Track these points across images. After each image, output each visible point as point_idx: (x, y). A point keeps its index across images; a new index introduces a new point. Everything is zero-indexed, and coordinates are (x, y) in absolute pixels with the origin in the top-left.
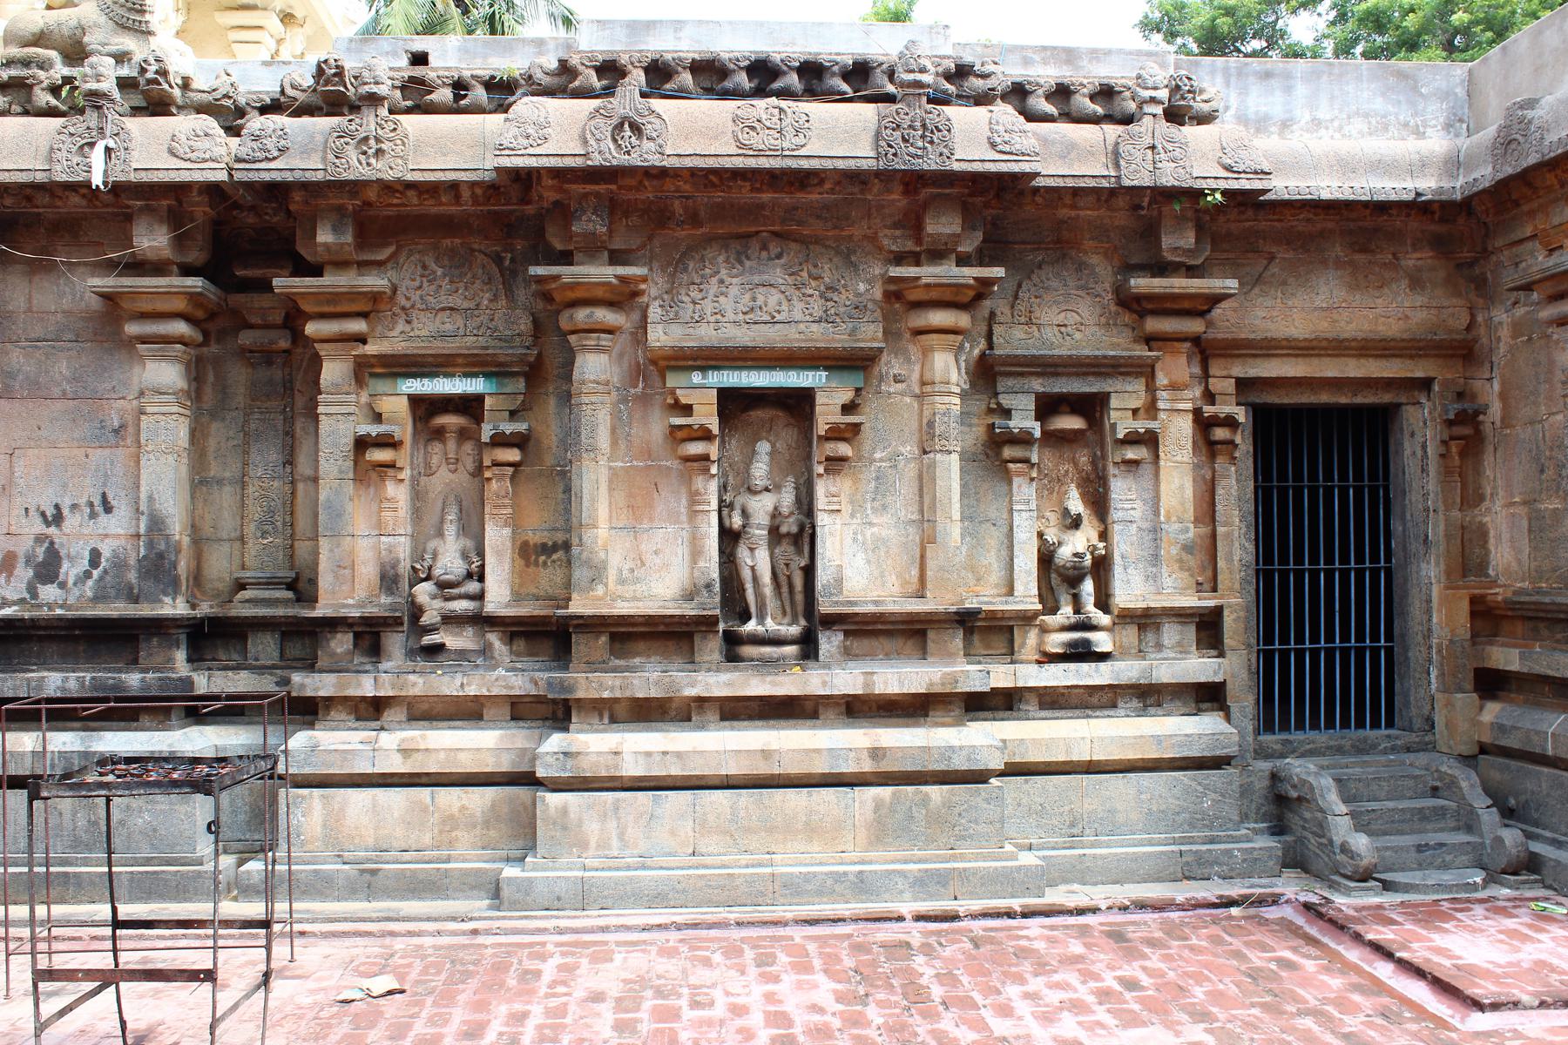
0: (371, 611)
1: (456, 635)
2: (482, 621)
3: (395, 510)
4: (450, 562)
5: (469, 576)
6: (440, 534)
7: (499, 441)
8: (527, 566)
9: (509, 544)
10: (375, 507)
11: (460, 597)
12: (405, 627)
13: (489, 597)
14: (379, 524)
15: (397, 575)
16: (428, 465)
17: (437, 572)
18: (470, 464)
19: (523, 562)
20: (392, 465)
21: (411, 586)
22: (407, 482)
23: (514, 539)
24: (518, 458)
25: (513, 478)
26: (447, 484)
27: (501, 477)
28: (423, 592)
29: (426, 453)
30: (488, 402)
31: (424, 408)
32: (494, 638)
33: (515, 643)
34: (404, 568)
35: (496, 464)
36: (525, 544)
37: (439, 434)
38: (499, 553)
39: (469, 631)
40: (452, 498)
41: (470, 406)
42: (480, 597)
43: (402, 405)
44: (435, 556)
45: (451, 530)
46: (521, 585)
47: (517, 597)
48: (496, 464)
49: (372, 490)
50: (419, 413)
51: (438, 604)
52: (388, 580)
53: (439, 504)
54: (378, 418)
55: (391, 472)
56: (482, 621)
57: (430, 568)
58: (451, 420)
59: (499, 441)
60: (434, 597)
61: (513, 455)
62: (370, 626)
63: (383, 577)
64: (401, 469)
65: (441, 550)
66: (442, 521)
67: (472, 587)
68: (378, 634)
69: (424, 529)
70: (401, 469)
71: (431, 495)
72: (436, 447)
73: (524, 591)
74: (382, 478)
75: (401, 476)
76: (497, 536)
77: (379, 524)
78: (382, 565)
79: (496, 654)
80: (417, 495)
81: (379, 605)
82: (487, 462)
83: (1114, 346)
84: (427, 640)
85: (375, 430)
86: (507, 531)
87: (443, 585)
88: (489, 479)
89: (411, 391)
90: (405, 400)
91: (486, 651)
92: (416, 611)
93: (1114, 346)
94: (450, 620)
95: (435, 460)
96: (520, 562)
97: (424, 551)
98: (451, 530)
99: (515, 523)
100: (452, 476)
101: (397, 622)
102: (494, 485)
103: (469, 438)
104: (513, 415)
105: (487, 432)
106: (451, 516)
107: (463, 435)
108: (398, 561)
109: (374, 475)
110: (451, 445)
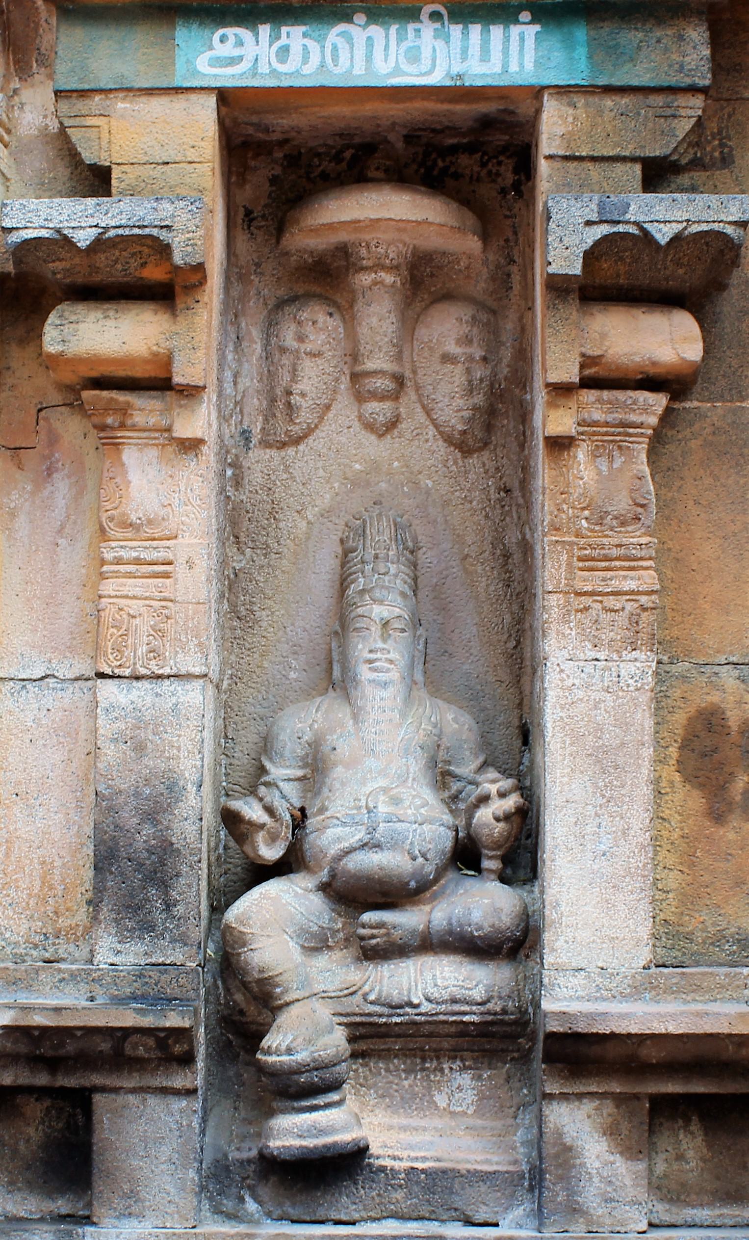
0: (58, 1002)
1: (405, 1102)
2: (518, 1047)
3: (163, 569)
4: (384, 792)
5: (465, 855)
6: (334, 675)
7: (622, 276)
8: (718, 817)
9: (644, 720)
10: (72, 560)
11: (429, 944)
12: (198, 1075)
13: (559, 947)
14: (93, 629)
15: (166, 850)
16: (279, 401)
17: (331, 837)
18: (451, 396)
19: (696, 801)
20: (158, 382)
21: (218, 909)
22: (209, 452)
23: (660, 704)
24: (694, 352)
25: (658, 441)
26: (357, 482)
27: (612, 437)
28: (276, 920)
29: (272, 352)
30: (555, 127)
31: (279, 160)
32: (580, 1125)
33: (664, 1141)
34: (193, 820)
35: (598, 378)
36: (709, 721)
37: (327, 277)
38: (604, 762)
39: (461, 1087)
40: (381, 535)
41: (474, 154)
42: (517, 944)
43: (195, 130)
44: (315, 769)
45: (383, 661)
46: (689, 899)
47: (676, 951)
48: (598, 378)
49: (61, 488)
50: (244, 196)
51: (334, 972)
52: (127, 870)
53: (325, 562)
54: (96, 181)
55: (146, 409)
56: (518, 1047)
57: (300, 819)
58: (385, 214)
59: (622, 276)
60: (317, 944)
61: (668, 339)
62: (53, 1064)
63: (107, 857)
64: (191, 393)
65: (343, 744)
66: (342, 621)
67: (483, 902)
68: (82, 1100)
69: (281, 643)
70: (191, 393)
71: (293, 525)
72: (316, 330)
73: (701, 922)
74: (108, 437)
75: (185, 429)
76: (594, 693)
77: (93, 629)
78: (105, 804)
79: (590, 1196)
80: (241, 525)
81: (88, 976)
82: (559, 363)
83: (488, 1162)
84: (294, 1131)
85: (81, 220)
86: (638, 667)
87: (355, 895)
88: (559, 445)
89: (231, 77)
90: (204, 115)
91: (540, 1177)
92: (244, 1006)
93: (488, 1162)
94: (381, 1039)
95: (312, 380)
96: (687, 800)
97: (266, 745)
98: (383, 661)
99: (666, 634)
100: (374, 447)
101: (171, 1049)
102: (584, 468)
103: (448, 297)
104: (657, 174)
105: (566, 232)
106: (384, 605)
107: (424, 281)
108: (173, 789)
109: (70, 428)
110: (379, 318)
